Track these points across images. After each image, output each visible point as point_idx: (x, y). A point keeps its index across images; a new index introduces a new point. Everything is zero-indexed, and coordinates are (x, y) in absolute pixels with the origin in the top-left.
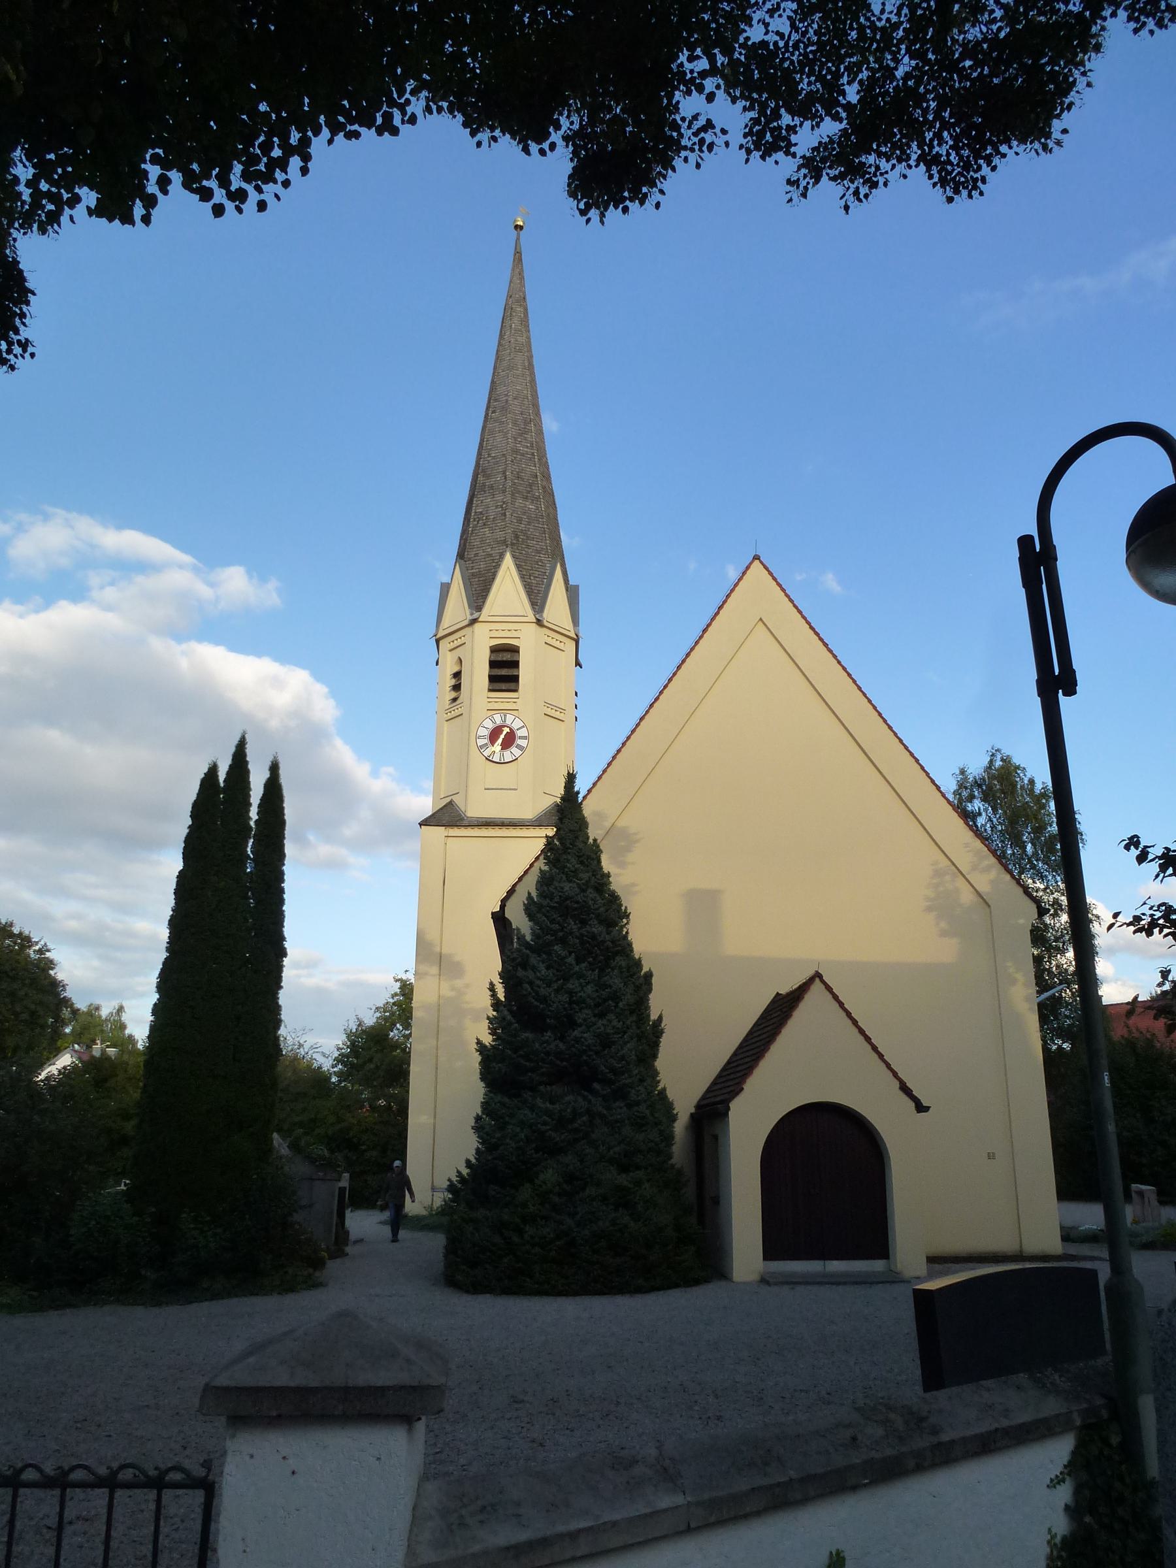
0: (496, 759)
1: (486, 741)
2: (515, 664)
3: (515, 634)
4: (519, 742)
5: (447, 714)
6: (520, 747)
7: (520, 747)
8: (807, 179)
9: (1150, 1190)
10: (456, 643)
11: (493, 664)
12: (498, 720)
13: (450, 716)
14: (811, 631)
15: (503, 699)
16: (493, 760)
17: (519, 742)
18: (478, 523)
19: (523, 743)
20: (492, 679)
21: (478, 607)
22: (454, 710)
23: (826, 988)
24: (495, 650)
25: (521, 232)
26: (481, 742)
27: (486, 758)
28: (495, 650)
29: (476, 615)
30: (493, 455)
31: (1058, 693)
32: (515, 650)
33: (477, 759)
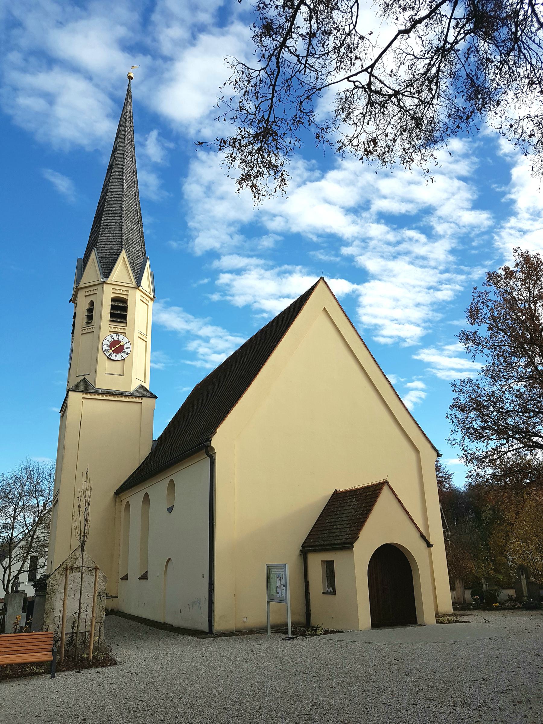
0: (113, 358)
1: (108, 348)
2: (125, 309)
3: (125, 293)
4: (126, 350)
5: (82, 330)
6: (126, 353)
7: (126, 353)
8: (279, 163)
9: (152, 273)
10: (90, 293)
11: (113, 307)
12: (115, 336)
13: (84, 332)
14: (359, 14)
15: (118, 327)
16: (111, 358)
17: (126, 350)
18: (105, 230)
19: (128, 351)
20: (112, 315)
21: (107, 275)
22: (87, 329)
23: (333, 631)
24: (114, 300)
25: (131, 81)
26: (105, 348)
27: (107, 357)
28: (114, 300)
29: (105, 279)
30: (114, 195)
31: (416, 360)
32: (125, 301)
33: (102, 357)
